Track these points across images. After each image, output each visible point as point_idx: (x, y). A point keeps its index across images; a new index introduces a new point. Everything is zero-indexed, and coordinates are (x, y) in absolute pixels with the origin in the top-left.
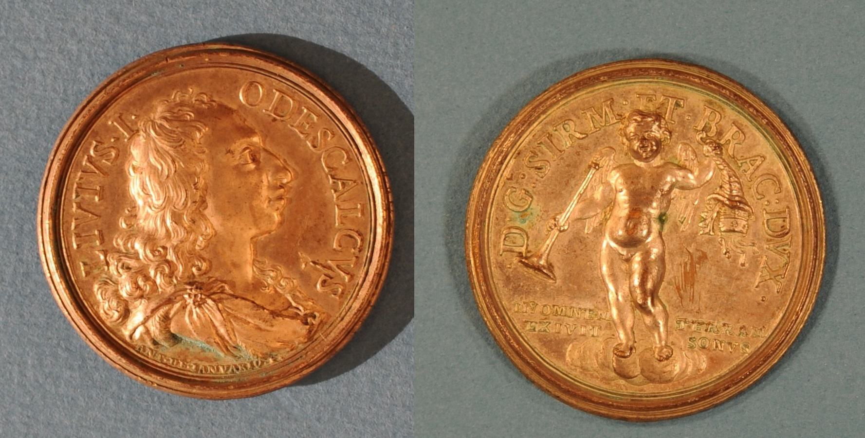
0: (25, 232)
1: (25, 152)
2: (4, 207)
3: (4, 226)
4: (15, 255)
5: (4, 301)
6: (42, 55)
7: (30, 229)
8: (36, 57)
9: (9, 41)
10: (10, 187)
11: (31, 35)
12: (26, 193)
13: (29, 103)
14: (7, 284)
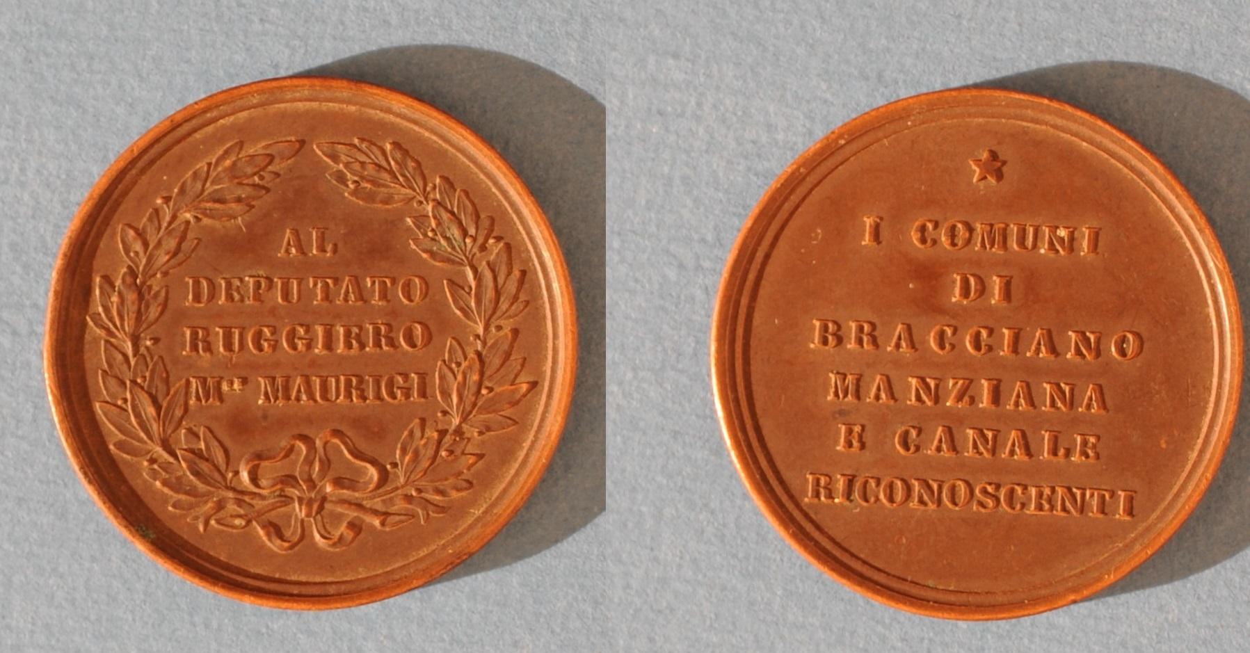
3: (635, 508)
6: (707, 264)
8: (698, 268)
11: (693, 234)
13: (683, 332)
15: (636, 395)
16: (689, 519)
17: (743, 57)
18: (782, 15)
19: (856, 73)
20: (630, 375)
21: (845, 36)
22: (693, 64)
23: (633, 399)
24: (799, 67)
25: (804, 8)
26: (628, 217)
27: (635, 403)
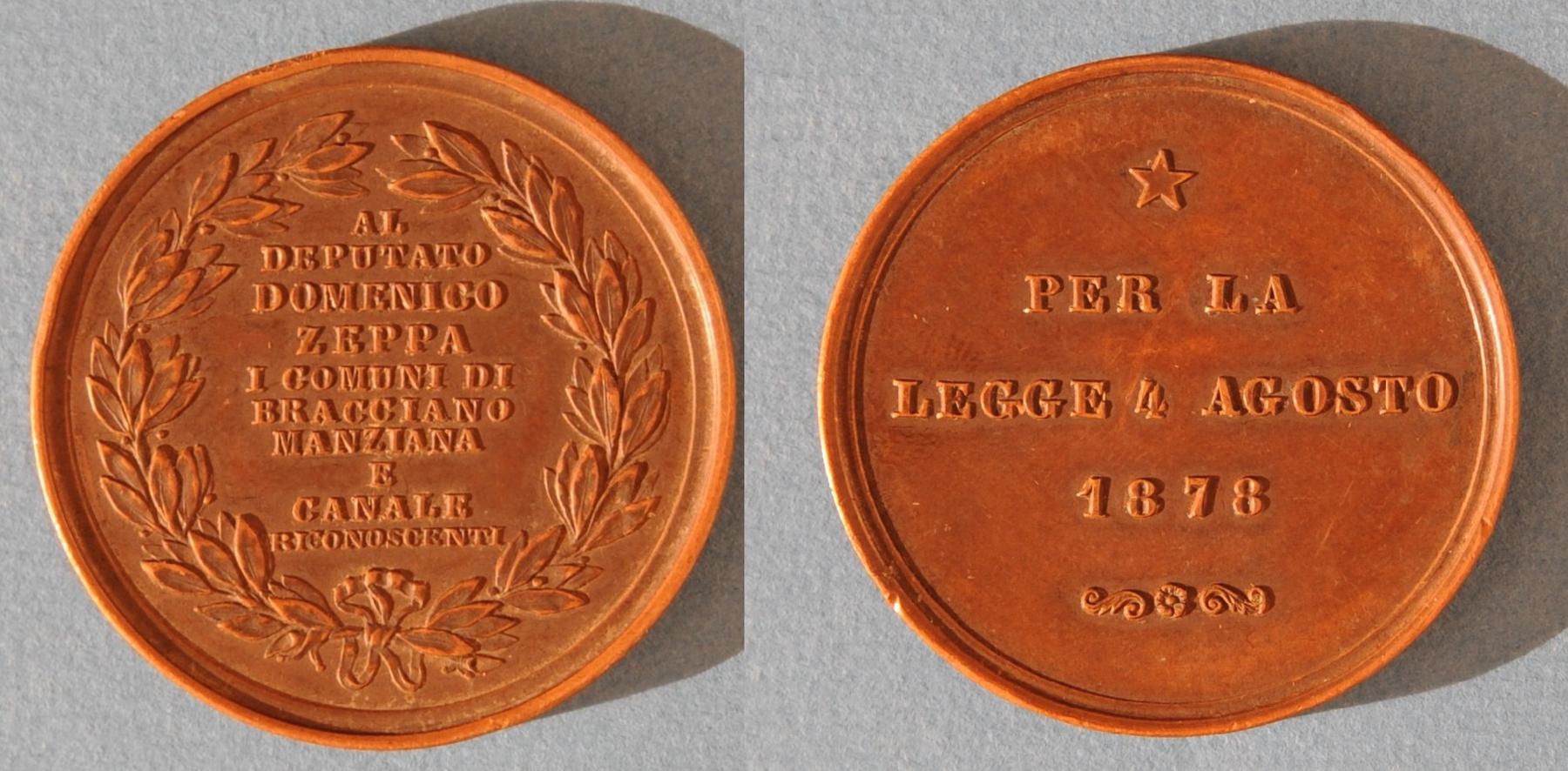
0: (834, 579)
1: (14, 520)
2: (797, 541)
3: (799, 572)
4: (820, 616)
5: (806, 691)
7: (841, 574)
9: (792, 278)
10: (807, 509)
11: (829, 266)
12: (22, 587)
14: (808, 664)
15: (785, 449)
16: (54, 647)
17: (22, 122)
18: (899, 17)
19: (989, 71)
20: (776, 427)
21: (972, 32)
22: (806, 81)
23: (782, 453)
24: (925, 71)
25: (79, 57)
26: (753, 256)
27: (785, 457)
